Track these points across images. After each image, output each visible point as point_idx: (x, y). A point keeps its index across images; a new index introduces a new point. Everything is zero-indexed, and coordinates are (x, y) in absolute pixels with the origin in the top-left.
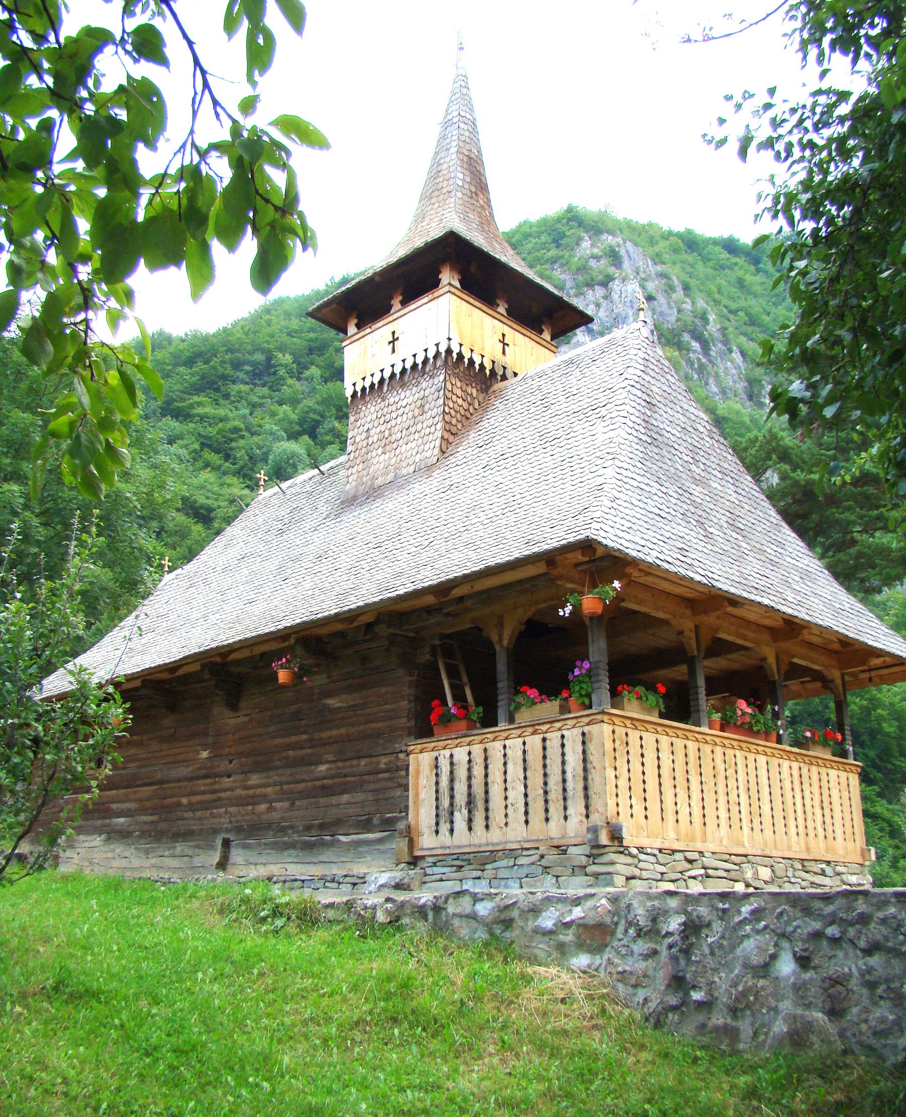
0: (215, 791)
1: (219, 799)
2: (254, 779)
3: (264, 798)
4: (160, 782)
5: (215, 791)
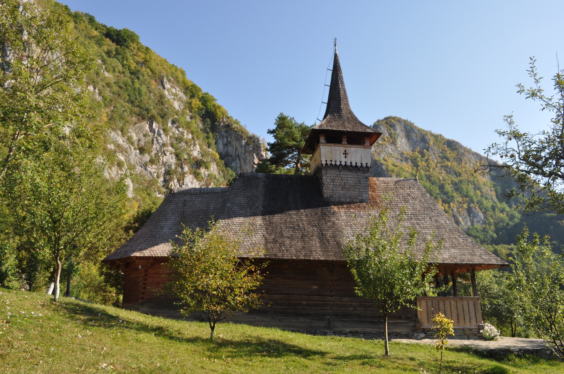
0: (323, 301)
1: (327, 304)
2: (346, 299)
3: (352, 306)
5: (323, 301)
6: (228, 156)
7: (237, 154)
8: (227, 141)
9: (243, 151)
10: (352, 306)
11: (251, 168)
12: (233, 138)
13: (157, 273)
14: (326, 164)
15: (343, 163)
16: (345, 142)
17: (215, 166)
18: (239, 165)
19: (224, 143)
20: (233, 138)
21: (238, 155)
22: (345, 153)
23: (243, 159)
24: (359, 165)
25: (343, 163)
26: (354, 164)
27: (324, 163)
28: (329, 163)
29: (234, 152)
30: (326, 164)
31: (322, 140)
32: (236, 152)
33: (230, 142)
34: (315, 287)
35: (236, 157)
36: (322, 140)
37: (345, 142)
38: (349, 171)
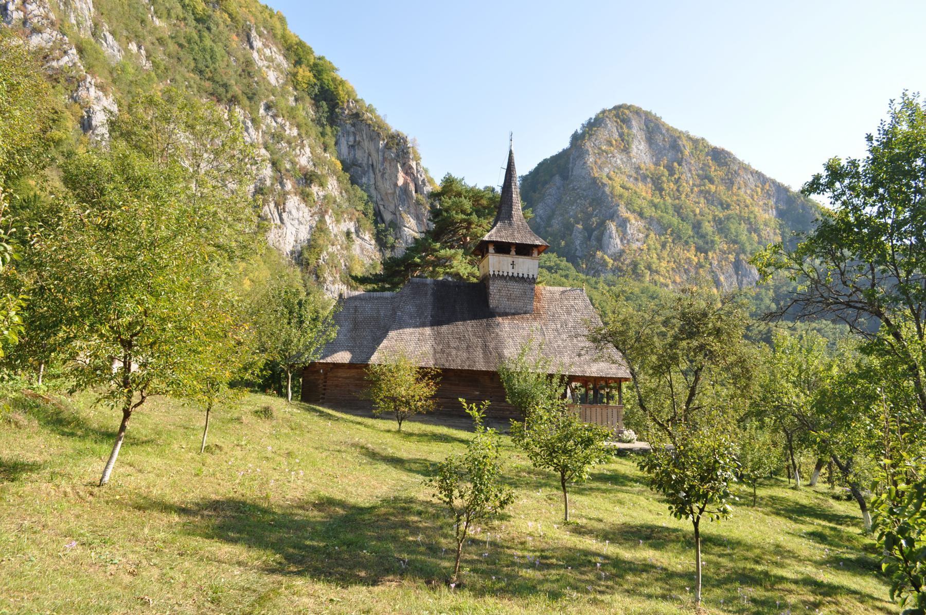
4: (453, 399)
6: (356, 165)
7: (370, 162)
8: (355, 141)
9: (381, 158)
10: (508, 410)
11: (392, 187)
12: (365, 136)
13: (335, 377)
14: (494, 274)
15: (510, 274)
16: (513, 252)
17: (335, 183)
18: (372, 182)
19: (350, 143)
20: (365, 136)
21: (372, 165)
22: (513, 264)
23: (380, 171)
24: (526, 276)
25: (510, 274)
26: (521, 275)
27: (492, 273)
28: (496, 273)
29: (365, 159)
30: (494, 274)
31: (491, 249)
32: (368, 159)
33: (359, 142)
34: (477, 393)
35: (368, 168)
36: (491, 249)
37: (513, 252)
38: (516, 281)
